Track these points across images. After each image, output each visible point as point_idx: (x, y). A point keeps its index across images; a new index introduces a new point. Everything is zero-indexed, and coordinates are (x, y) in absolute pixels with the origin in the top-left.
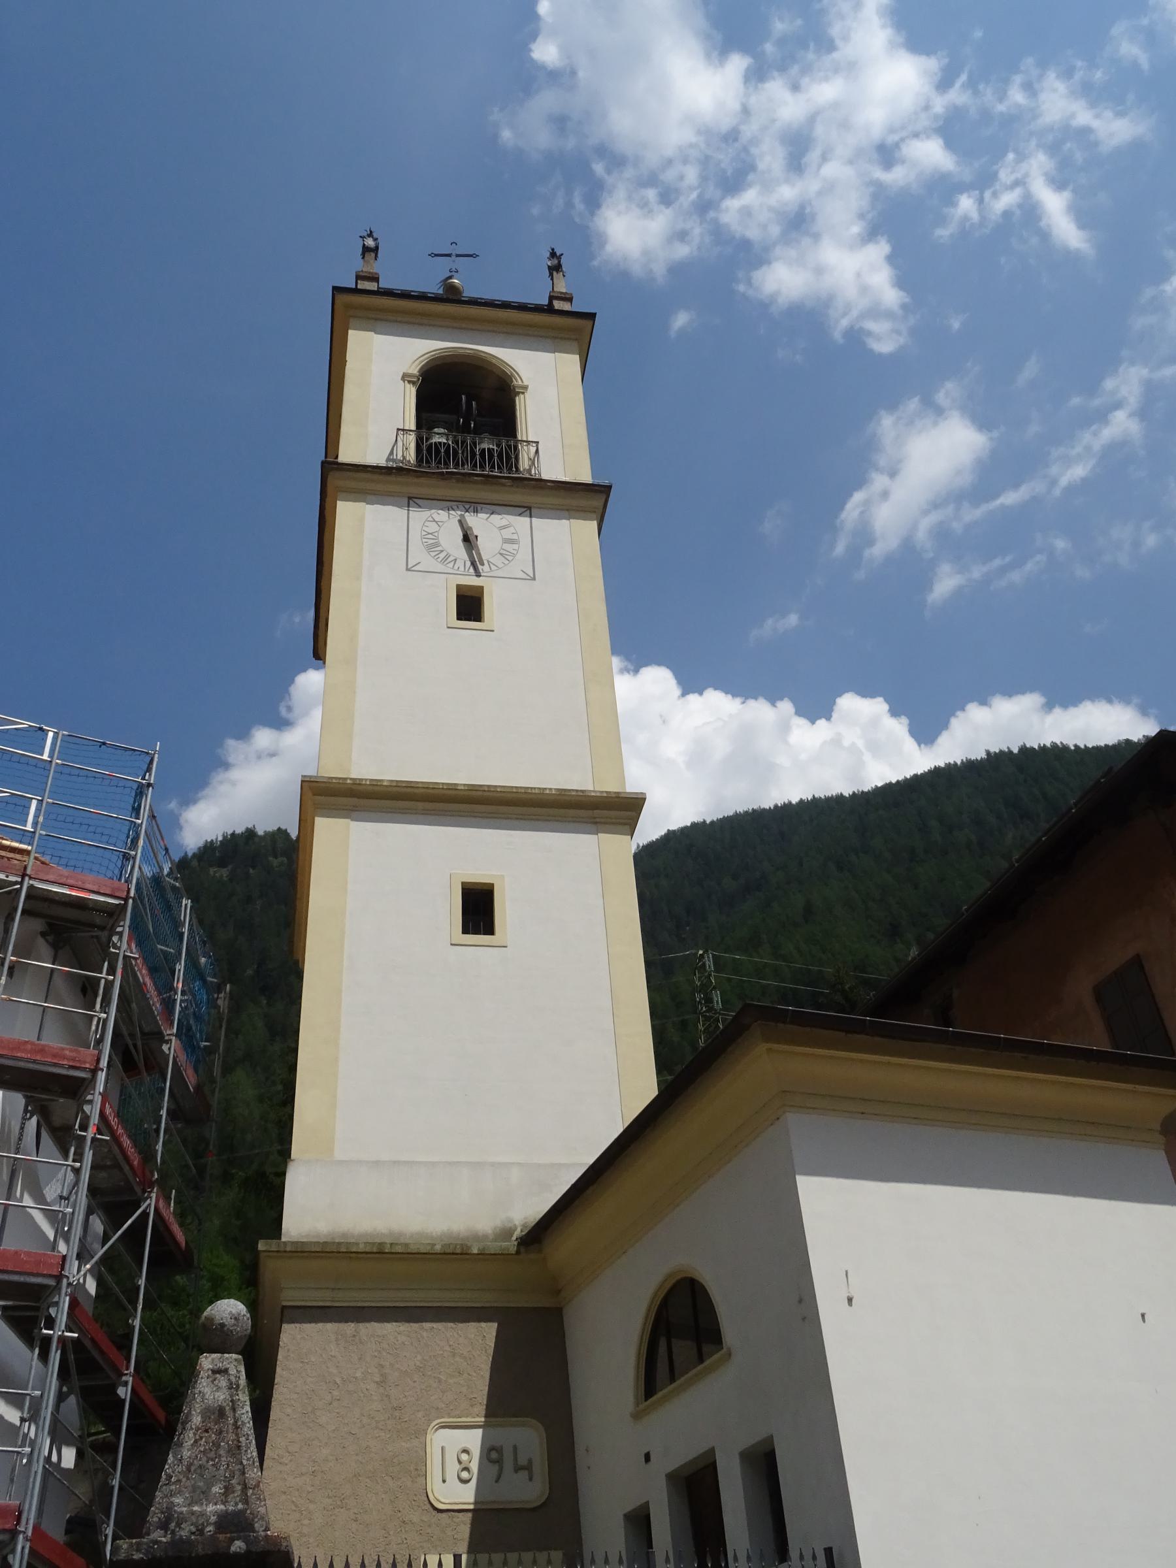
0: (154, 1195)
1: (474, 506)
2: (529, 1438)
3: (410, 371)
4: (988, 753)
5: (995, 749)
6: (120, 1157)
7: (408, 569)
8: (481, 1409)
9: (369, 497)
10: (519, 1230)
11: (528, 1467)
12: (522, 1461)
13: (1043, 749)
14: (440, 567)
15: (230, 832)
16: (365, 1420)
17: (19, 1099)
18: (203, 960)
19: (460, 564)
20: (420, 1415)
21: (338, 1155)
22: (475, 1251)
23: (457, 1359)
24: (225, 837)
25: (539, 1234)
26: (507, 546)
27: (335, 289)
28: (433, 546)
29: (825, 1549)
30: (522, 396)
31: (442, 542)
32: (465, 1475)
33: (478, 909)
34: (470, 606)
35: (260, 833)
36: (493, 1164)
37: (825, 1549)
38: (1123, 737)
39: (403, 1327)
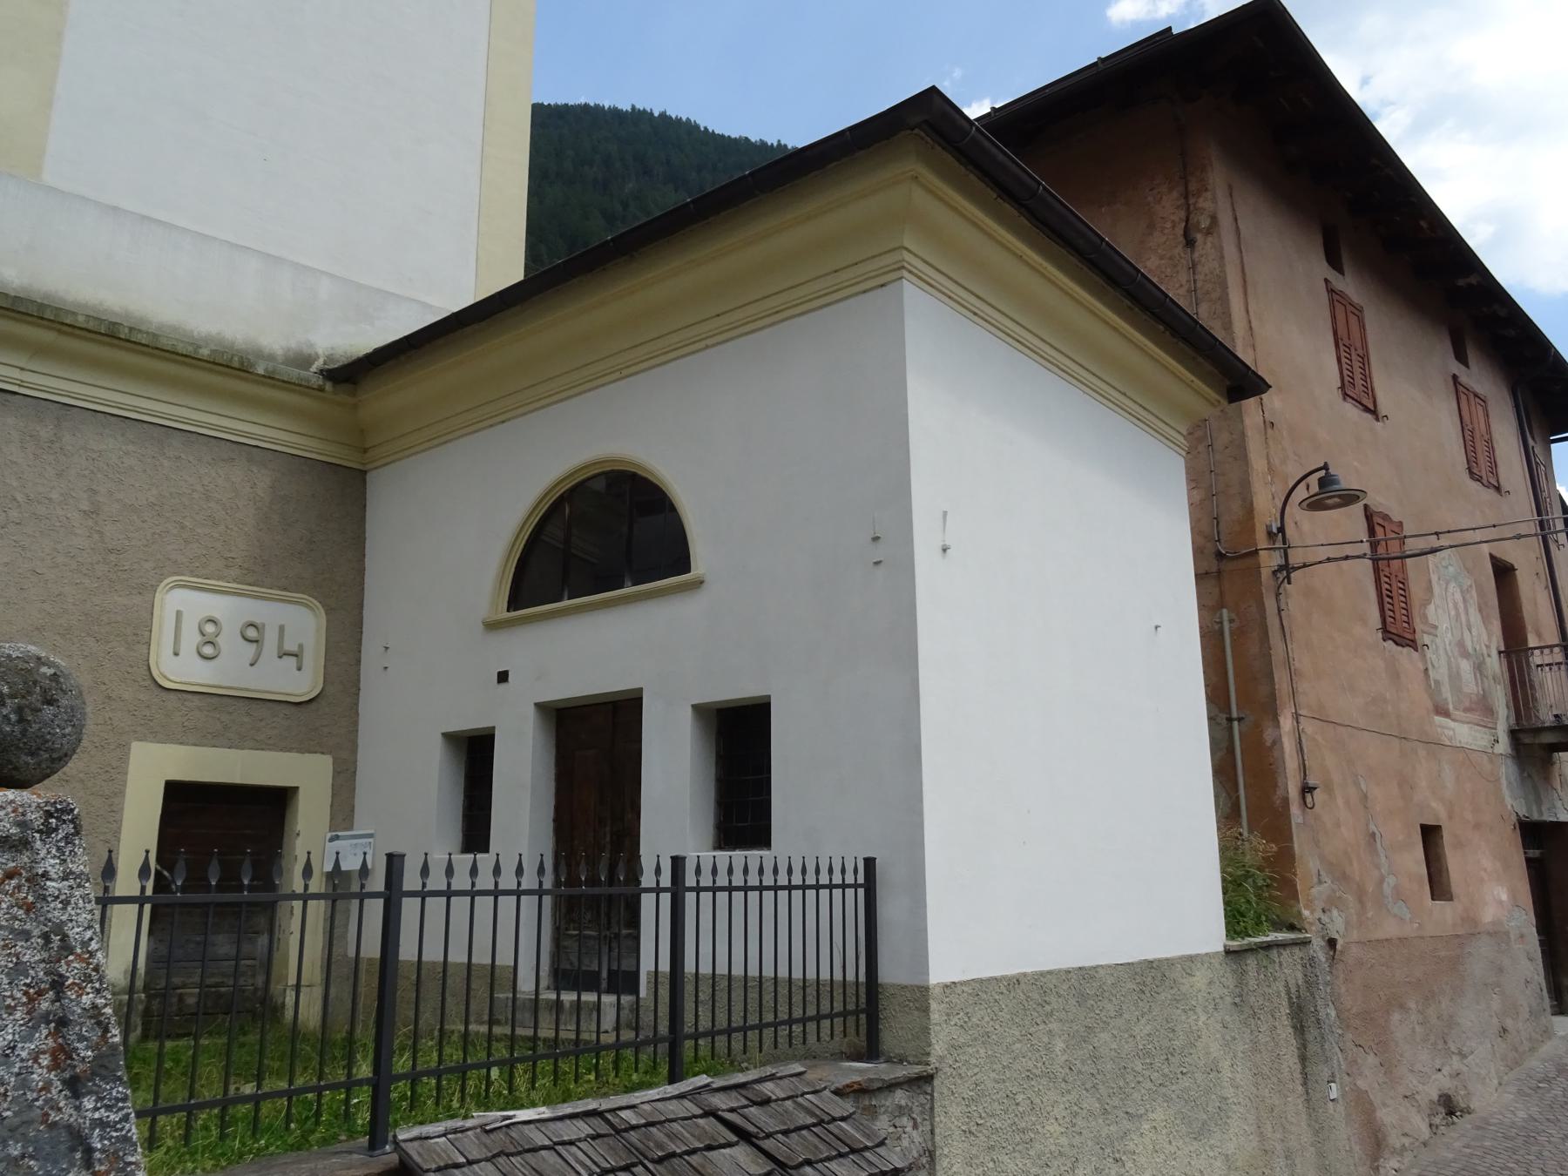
4: (633, 107)
5: (640, 106)
10: (321, 361)
12: (290, 646)
13: (679, 120)
21: (48, 178)
22: (261, 371)
25: (352, 375)
29: (453, 739)
32: (208, 650)
37: (453, 739)
38: (744, 135)
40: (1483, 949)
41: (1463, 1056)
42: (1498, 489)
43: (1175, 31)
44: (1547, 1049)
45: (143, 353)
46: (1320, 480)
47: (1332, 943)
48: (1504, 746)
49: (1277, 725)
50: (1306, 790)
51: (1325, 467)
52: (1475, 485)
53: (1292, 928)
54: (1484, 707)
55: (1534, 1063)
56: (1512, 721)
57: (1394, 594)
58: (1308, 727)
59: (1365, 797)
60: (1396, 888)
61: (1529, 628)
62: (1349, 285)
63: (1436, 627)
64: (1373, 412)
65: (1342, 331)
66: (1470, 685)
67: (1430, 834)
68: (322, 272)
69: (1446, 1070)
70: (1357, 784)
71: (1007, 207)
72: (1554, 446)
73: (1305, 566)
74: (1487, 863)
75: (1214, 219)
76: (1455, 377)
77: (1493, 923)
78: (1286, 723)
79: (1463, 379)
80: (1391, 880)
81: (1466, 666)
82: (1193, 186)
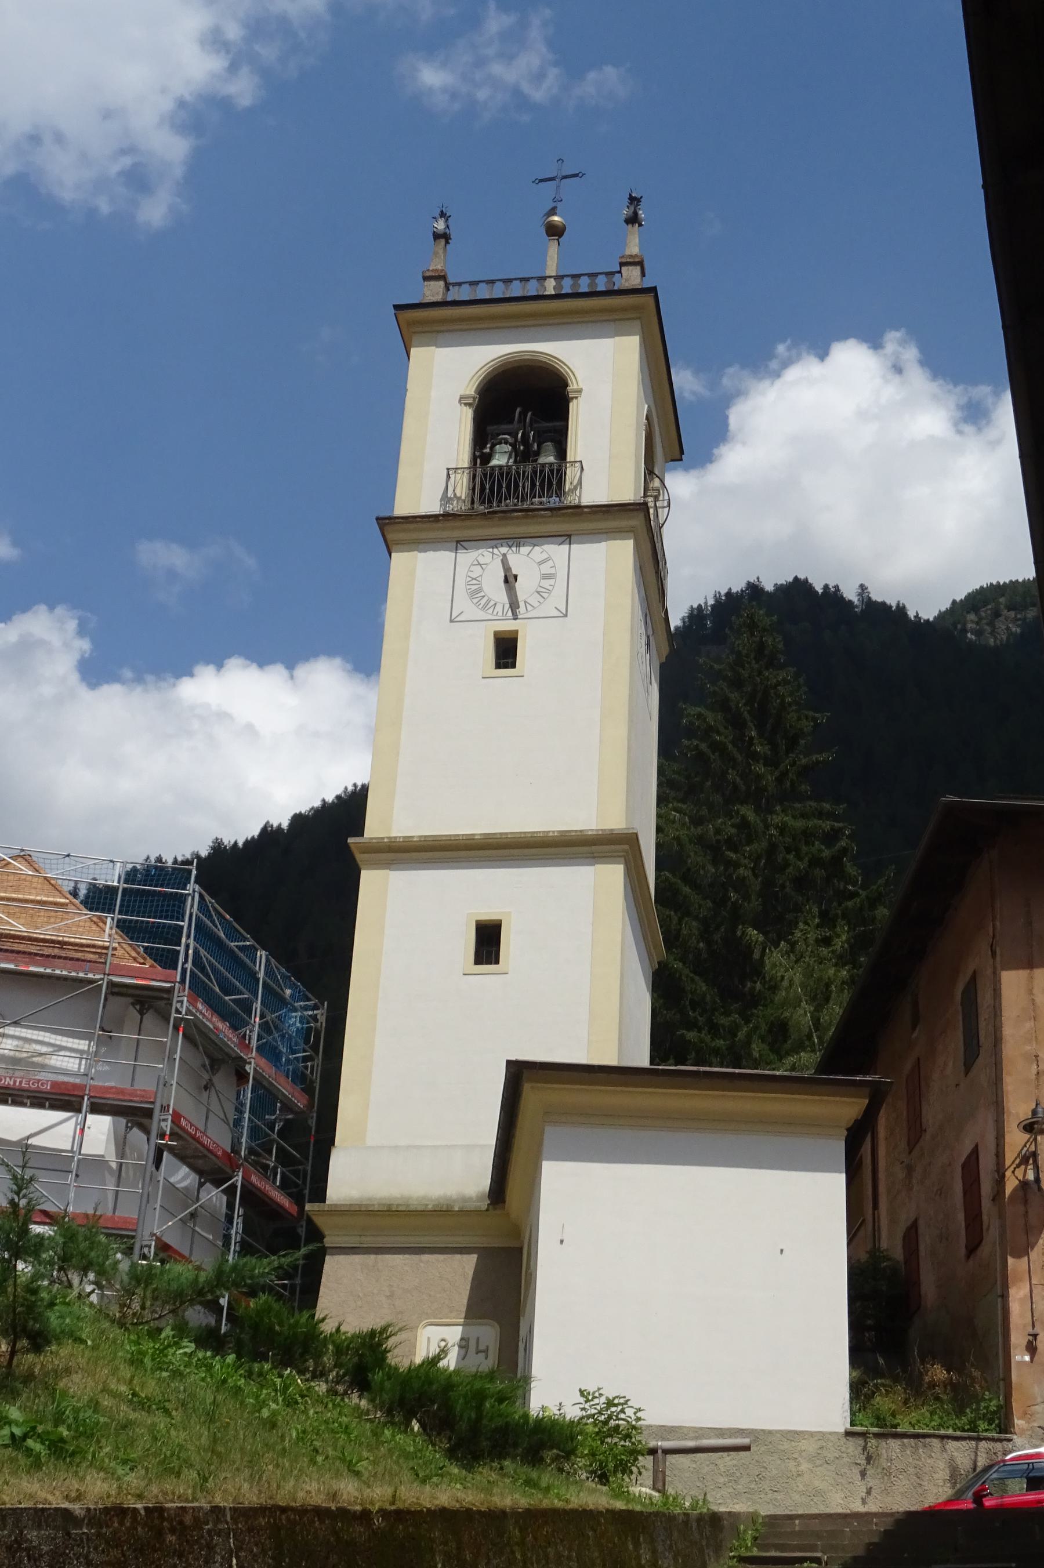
0: (240, 1174)
1: (516, 540)
2: (489, 1334)
3: (468, 393)
6: (206, 1152)
7: (451, 621)
8: (463, 1315)
9: (421, 546)
11: (486, 1351)
12: (482, 1347)
14: (481, 615)
15: (723, 592)
17: (123, 1121)
18: (288, 992)
19: (499, 608)
21: (369, 1142)
24: (718, 600)
26: (546, 583)
27: (397, 307)
28: (476, 593)
30: (575, 401)
31: (485, 588)
33: (488, 942)
34: (506, 652)
35: (769, 587)
39: (441, 1257)
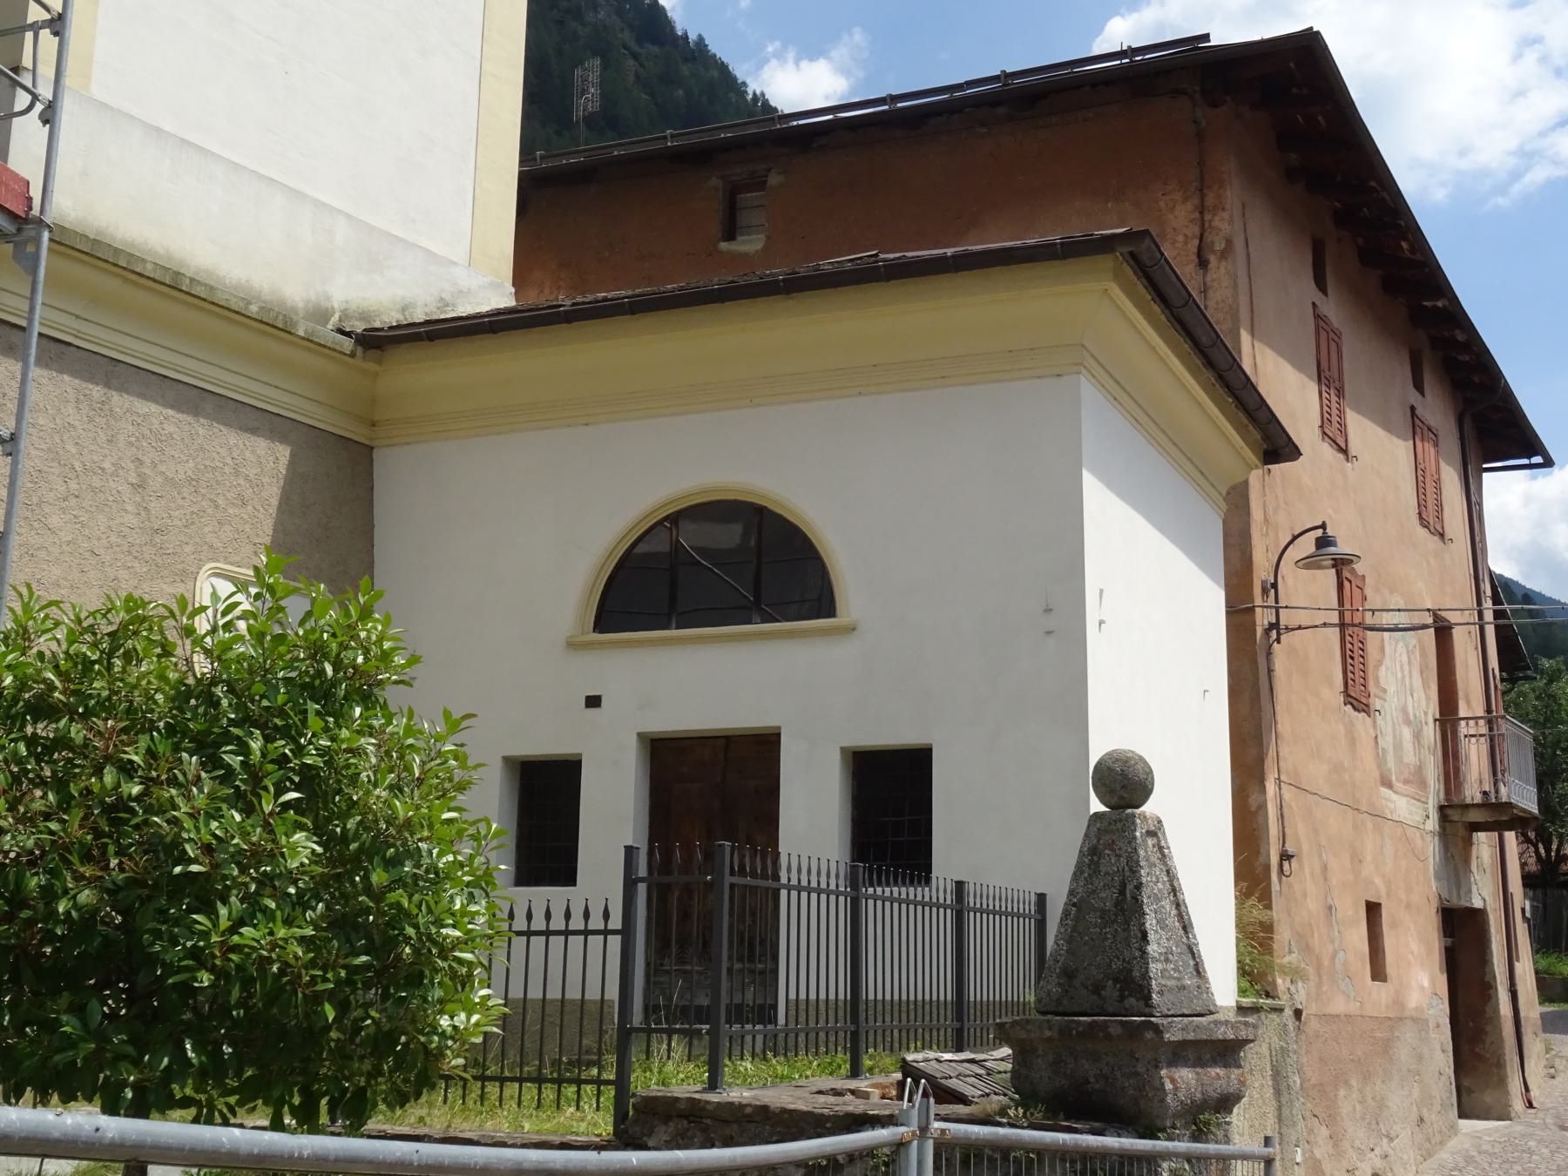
10: (337, 316)
16: (113, 539)
20: (188, 549)
22: (301, 333)
23: (241, 482)
25: (378, 342)
36: (317, 203)
40: (1408, 1035)
41: (1391, 1140)
42: (1442, 535)
43: (1214, 42)
44: (1453, 1144)
45: (102, 270)
46: (1318, 539)
47: (1298, 1013)
48: (1432, 824)
49: (1263, 790)
50: (1285, 856)
51: (1323, 526)
52: (1422, 532)
53: (1268, 995)
54: (1419, 779)
55: (1444, 1155)
56: (1442, 795)
57: (1356, 655)
58: (1288, 793)
59: (1325, 868)
60: (1345, 964)
61: (1461, 694)
62: (1332, 309)
63: (1385, 691)
64: (1344, 451)
65: (1324, 364)
66: (1410, 757)
67: (1373, 909)
68: (340, 212)
69: (1378, 1151)
70: (1320, 856)
71: (1156, 308)
72: (1485, 475)
73: (1300, 628)
74: (1414, 946)
75: (1229, 242)
76: (1413, 408)
77: (1416, 1008)
78: (1271, 787)
79: (1419, 411)
80: (1341, 955)
81: (1407, 733)
82: (1210, 200)
